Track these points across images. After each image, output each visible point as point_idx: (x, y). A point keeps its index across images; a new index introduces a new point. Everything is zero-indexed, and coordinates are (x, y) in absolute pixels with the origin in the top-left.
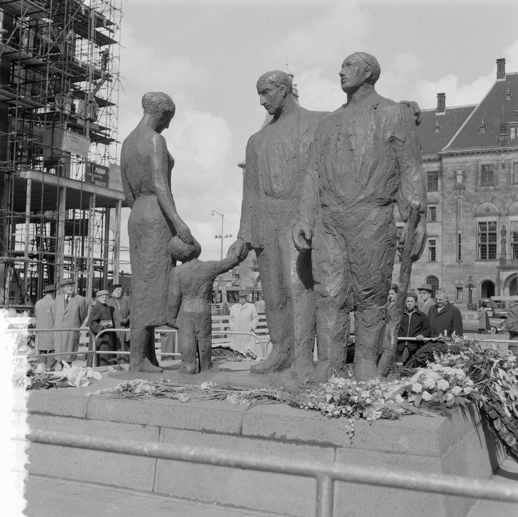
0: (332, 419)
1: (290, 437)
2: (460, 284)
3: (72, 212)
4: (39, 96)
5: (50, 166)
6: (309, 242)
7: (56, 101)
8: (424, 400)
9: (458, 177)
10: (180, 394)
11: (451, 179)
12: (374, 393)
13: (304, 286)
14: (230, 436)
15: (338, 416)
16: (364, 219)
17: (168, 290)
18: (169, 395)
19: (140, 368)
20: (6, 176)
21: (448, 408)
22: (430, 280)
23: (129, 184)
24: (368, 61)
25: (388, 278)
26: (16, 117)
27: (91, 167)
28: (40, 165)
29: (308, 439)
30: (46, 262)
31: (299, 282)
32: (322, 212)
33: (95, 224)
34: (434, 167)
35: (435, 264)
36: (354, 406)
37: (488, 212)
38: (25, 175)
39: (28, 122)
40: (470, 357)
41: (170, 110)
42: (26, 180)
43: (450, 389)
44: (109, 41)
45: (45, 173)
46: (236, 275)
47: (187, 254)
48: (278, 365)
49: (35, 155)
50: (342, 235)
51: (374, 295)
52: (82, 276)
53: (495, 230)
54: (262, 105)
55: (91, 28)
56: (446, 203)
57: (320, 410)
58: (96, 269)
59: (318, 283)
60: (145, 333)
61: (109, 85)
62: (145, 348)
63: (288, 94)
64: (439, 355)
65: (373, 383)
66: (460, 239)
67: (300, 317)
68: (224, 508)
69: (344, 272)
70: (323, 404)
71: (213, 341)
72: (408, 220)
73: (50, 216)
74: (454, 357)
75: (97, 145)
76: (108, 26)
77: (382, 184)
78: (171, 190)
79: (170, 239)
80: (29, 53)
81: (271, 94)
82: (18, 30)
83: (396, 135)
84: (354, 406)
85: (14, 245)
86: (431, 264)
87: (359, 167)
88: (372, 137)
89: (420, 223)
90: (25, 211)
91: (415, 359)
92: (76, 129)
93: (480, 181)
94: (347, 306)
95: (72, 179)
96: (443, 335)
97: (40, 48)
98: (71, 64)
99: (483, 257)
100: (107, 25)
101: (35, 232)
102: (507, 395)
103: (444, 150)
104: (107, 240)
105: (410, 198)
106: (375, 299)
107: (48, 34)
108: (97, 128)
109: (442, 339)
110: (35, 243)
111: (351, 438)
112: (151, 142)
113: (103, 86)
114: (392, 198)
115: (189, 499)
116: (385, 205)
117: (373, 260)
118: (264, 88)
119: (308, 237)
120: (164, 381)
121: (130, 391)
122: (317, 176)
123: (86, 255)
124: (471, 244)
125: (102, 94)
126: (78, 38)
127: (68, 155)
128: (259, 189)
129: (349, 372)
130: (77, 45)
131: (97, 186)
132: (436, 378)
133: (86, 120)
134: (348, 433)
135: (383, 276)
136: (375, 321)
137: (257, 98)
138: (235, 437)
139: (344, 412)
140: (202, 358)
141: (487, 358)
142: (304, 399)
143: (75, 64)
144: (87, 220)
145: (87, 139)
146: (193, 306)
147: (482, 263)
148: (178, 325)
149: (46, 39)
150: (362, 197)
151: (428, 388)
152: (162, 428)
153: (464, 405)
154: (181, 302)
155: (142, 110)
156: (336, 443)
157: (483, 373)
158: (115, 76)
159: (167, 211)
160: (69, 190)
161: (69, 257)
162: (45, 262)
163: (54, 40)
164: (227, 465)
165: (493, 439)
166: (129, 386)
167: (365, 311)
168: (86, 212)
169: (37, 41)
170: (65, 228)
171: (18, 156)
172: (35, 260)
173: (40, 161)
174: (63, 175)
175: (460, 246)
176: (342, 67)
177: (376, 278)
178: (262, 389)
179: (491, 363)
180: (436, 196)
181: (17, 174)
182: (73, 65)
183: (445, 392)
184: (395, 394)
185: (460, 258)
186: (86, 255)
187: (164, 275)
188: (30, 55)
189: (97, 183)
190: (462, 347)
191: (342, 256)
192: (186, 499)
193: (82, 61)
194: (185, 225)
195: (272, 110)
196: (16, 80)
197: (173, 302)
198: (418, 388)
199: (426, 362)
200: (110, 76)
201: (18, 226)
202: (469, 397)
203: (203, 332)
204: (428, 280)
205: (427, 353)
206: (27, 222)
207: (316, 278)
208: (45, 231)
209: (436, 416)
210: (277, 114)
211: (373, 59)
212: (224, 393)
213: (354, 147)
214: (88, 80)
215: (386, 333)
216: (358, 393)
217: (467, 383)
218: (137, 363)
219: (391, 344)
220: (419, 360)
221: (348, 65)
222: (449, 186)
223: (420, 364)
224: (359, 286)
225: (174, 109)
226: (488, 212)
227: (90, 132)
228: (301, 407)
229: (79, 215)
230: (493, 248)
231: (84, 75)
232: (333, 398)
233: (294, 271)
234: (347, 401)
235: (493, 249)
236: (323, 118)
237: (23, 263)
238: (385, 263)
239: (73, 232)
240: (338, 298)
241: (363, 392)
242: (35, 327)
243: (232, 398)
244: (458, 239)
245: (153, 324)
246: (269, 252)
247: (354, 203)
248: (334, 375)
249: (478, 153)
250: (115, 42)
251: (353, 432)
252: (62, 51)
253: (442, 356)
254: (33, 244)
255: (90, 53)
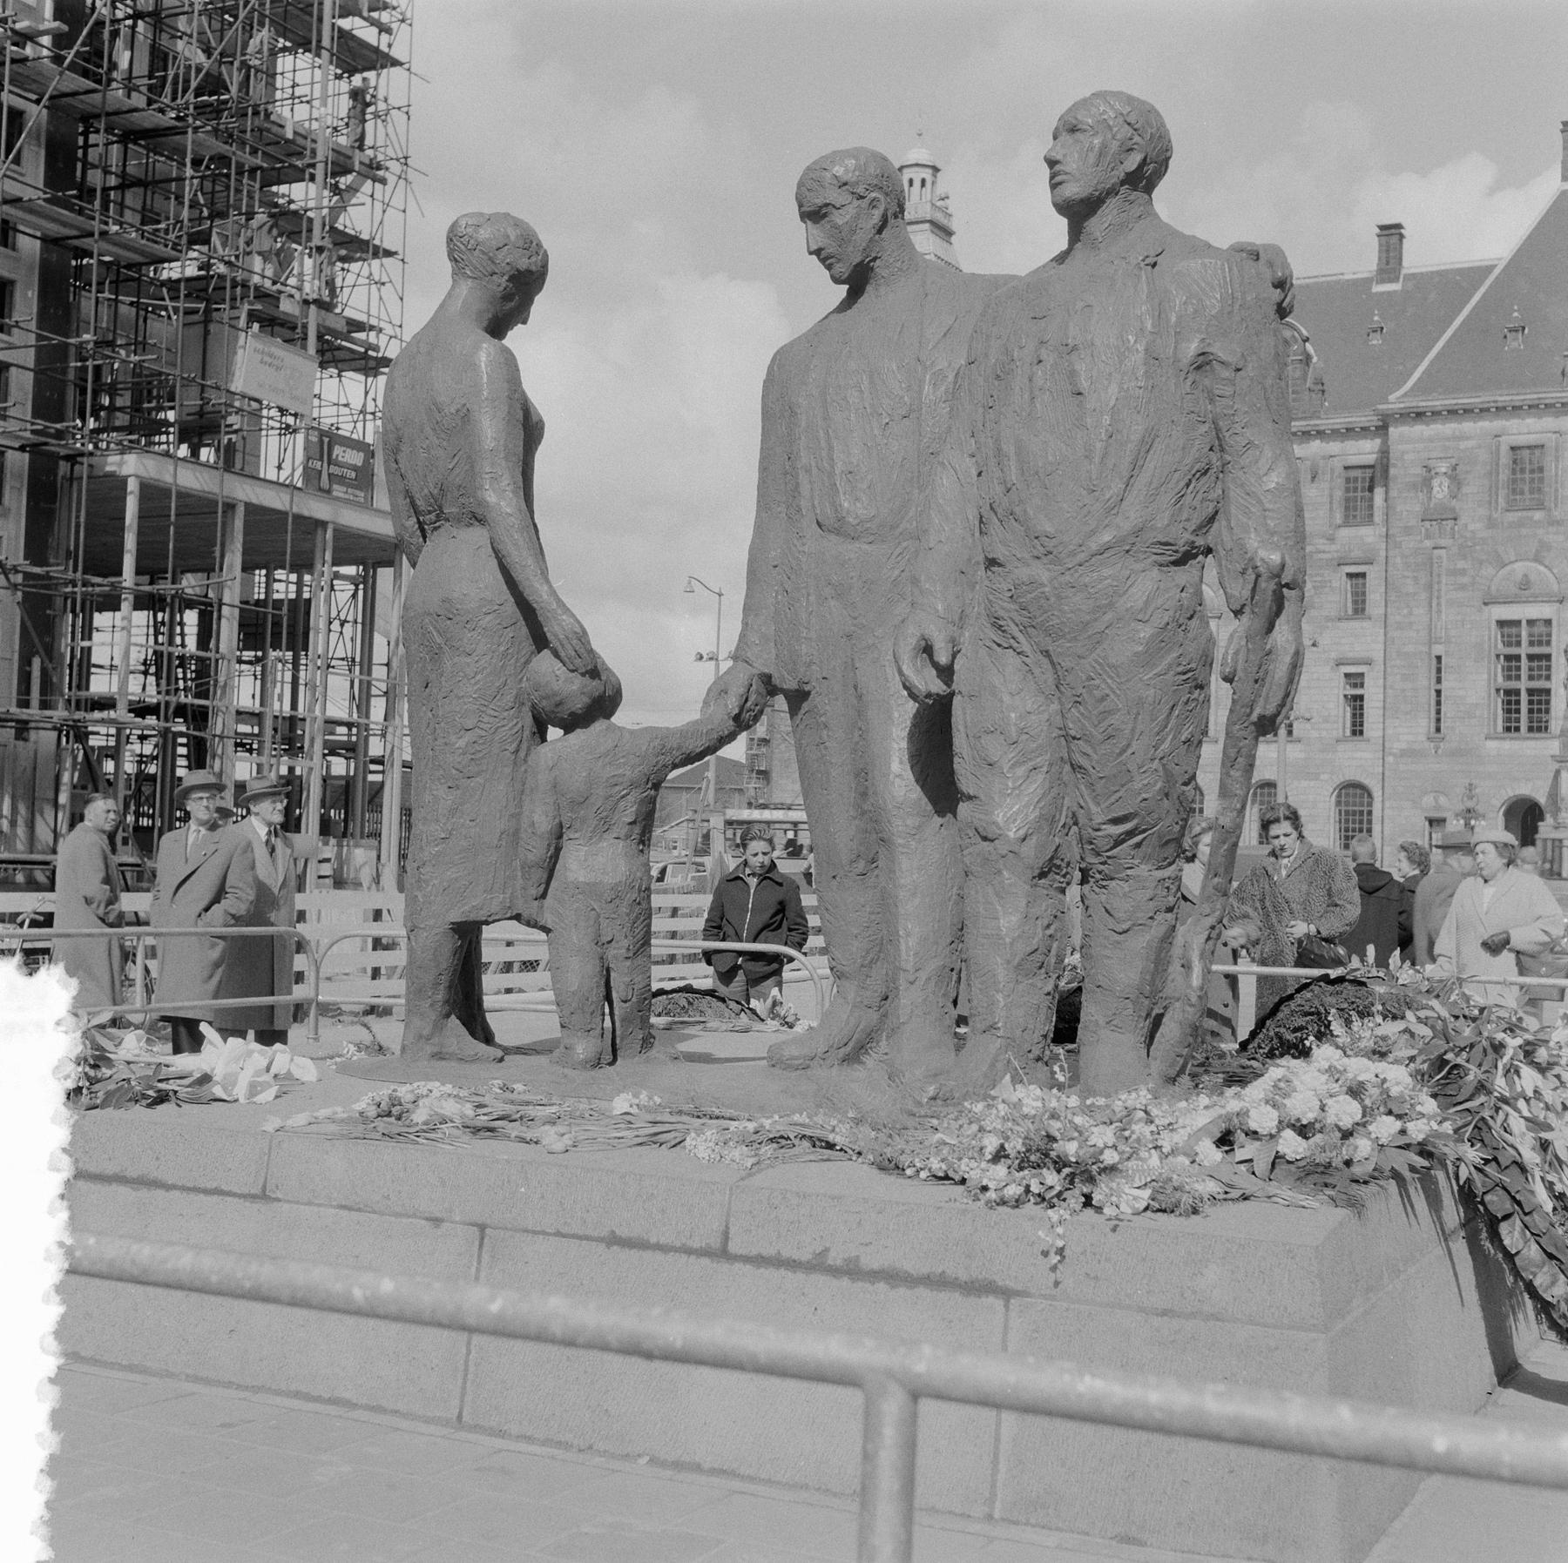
0: (1000, 1208)
1: (871, 1261)
2: (1438, 807)
3: (263, 579)
4: (162, 226)
5: (196, 440)
6: (946, 673)
7: (215, 239)
8: (1283, 1157)
9: (1435, 483)
10: (547, 1127)
11: (1414, 486)
12: (1127, 1133)
13: (930, 807)
14: (693, 1257)
15: (1018, 1203)
16: (1111, 605)
17: (519, 814)
18: (514, 1129)
19: (436, 1050)
20: (64, 467)
21: (1357, 1181)
22: (1347, 795)
23: (408, 494)
24: (1131, 119)
25: (1186, 784)
26: (94, 288)
27: (321, 442)
28: (168, 433)
29: (925, 1271)
30: (183, 729)
31: (916, 793)
32: (987, 583)
33: (334, 615)
34: (1365, 450)
35: (1363, 745)
36: (1066, 1171)
37: (1525, 590)
38: (120, 464)
39: (132, 304)
40: (1433, 1028)
41: (534, 268)
42: (123, 481)
43: (1364, 1125)
44: (379, 60)
45: (184, 459)
46: (759, 772)
47: (578, 704)
48: (851, 1044)
49: (153, 404)
50: (1047, 654)
51: (1140, 837)
52: (291, 770)
53: (1548, 643)
54: (811, 253)
55: (320, 20)
56: (1398, 560)
57: (963, 1181)
58: (332, 749)
59: (970, 798)
60: (449, 944)
61: (378, 195)
62: (450, 987)
63: (892, 221)
64: (1348, 1023)
65: (1129, 1104)
66: (1439, 670)
67: (917, 901)
68: (669, 1473)
69: (1051, 765)
70: (973, 1164)
71: (657, 971)
72: (1247, 609)
73: (198, 591)
74: (1391, 1028)
75: (339, 376)
76: (375, 15)
77: (1166, 499)
78: (531, 512)
79: (527, 662)
80: (134, 94)
81: (839, 218)
82: (100, 24)
83: (1218, 349)
84: (1066, 1171)
85: (89, 674)
86: (1350, 745)
87: (1099, 445)
88: (1141, 355)
89: (1283, 617)
90: (120, 574)
91: (1276, 1034)
92: (277, 329)
93: (1502, 493)
94: (1059, 867)
95: (265, 480)
96: (1362, 961)
97: (170, 78)
98: (261, 130)
99: (1511, 728)
100: (371, 10)
101: (152, 639)
102: (1544, 1146)
103: (1396, 401)
104: (367, 664)
105: (1252, 542)
106: (1143, 848)
107: (191, 36)
108: (341, 326)
109: (1358, 974)
110: (153, 669)
111: (1054, 1269)
112: (474, 367)
113: (360, 197)
114: (1200, 542)
115: (566, 1446)
116: (1176, 563)
117: (1138, 731)
118: (819, 201)
119: (943, 659)
120: (505, 1088)
121: (399, 1118)
122: (974, 473)
123: (301, 710)
124: (1475, 688)
125: (357, 220)
126: (284, 49)
127: (255, 405)
128: (799, 510)
129: (1056, 1068)
130: (279, 70)
131: (337, 499)
132: (1322, 1089)
133: (306, 302)
134: (1045, 1254)
135: (1169, 777)
136: (1142, 917)
137: (798, 233)
138: (705, 1261)
139: (1035, 1188)
140: (623, 1020)
141: (1486, 1034)
142: (917, 1147)
143: (275, 129)
144: (309, 601)
145: (310, 358)
146: (594, 862)
147: (1510, 746)
148: (548, 919)
149: (187, 54)
150: (1106, 537)
151: (1298, 1120)
152: (488, 1231)
153: (1407, 1174)
154: (558, 850)
155: (448, 266)
156: (1011, 1284)
157: (1471, 1077)
158: (395, 167)
159: (518, 575)
160: (253, 510)
161: (252, 714)
162: (179, 726)
163: (209, 55)
164: (601, 1345)
165: (1500, 1283)
166: (395, 1101)
167: (1113, 884)
168: (307, 578)
169: (159, 58)
170: (241, 625)
171: (103, 408)
172: (151, 720)
173: (166, 423)
174: (238, 465)
175: (1439, 692)
176: (1055, 138)
177: (1146, 784)
178: (796, 1118)
179: (1498, 1048)
180: (1370, 540)
181: (94, 460)
182: (268, 131)
183: (1347, 1135)
184: (1197, 1135)
185: (1438, 730)
186: (301, 710)
187: (507, 770)
188: (139, 100)
189: (338, 490)
190: (1419, 998)
191: (1046, 716)
192: (559, 1444)
193: (296, 119)
194: (573, 616)
195: (843, 269)
196: (95, 178)
197: (536, 850)
198: (1263, 1119)
199: (1307, 1043)
200: (379, 167)
201: (101, 619)
202: (1424, 1150)
203: (625, 943)
204: (1339, 796)
205: (1311, 1014)
206: (126, 606)
207: (966, 783)
208: (182, 635)
209: (1316, 1205)
210: (858, 281)
211: (1150, 111)
212: (679, 1126)
213: (1084, 384)
214: (312, 178)
215: (1176, 951)
216: (1081, 1133)
217: (1419, 1108)
218: (425, 1032)
219: (1190, 986)
220: (1290, 1037)
221: (1073, 130)
222: (1409, 507)
223: (1289, 1048)
224: (1094, 808)
225: (545, 266)
226: (1525, 590)
227: (320, 337)
228: (909, 1172)
229: (284, 586)
230: (1541, 698)
231: (299, 163)
232: (1002, 1147)
233: (901, 762)
234: (1047, 1155)
235: (1540, 702)
236: (1000, 294)
237: (113, 731)
238: (1174, 738)
239: (264, 639)
240: (1032, 841)
241: (1094, 1129)
242: (147, 924)
243: (702, 1143)
244: (1434, 671)
245: (472, 917)
246: (828, 703)
247: (1081, 557)
248: (1008, 1077)
249: (1501, 410)
250: (396, 63)
251: (1060, 1251)
252: (234, 89)
253: (1356, 1025)
254: (146, 673)
255: (317, 94)
